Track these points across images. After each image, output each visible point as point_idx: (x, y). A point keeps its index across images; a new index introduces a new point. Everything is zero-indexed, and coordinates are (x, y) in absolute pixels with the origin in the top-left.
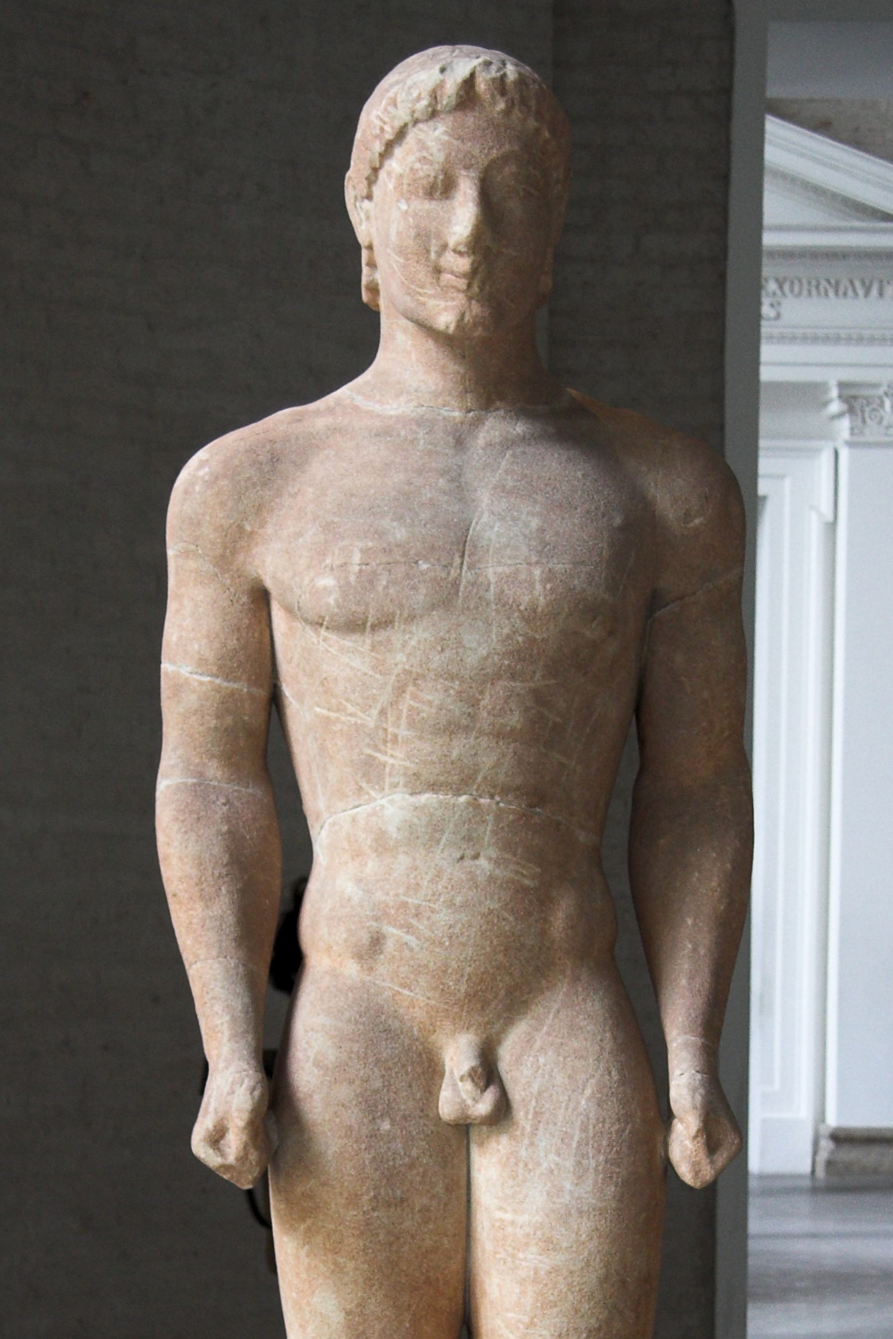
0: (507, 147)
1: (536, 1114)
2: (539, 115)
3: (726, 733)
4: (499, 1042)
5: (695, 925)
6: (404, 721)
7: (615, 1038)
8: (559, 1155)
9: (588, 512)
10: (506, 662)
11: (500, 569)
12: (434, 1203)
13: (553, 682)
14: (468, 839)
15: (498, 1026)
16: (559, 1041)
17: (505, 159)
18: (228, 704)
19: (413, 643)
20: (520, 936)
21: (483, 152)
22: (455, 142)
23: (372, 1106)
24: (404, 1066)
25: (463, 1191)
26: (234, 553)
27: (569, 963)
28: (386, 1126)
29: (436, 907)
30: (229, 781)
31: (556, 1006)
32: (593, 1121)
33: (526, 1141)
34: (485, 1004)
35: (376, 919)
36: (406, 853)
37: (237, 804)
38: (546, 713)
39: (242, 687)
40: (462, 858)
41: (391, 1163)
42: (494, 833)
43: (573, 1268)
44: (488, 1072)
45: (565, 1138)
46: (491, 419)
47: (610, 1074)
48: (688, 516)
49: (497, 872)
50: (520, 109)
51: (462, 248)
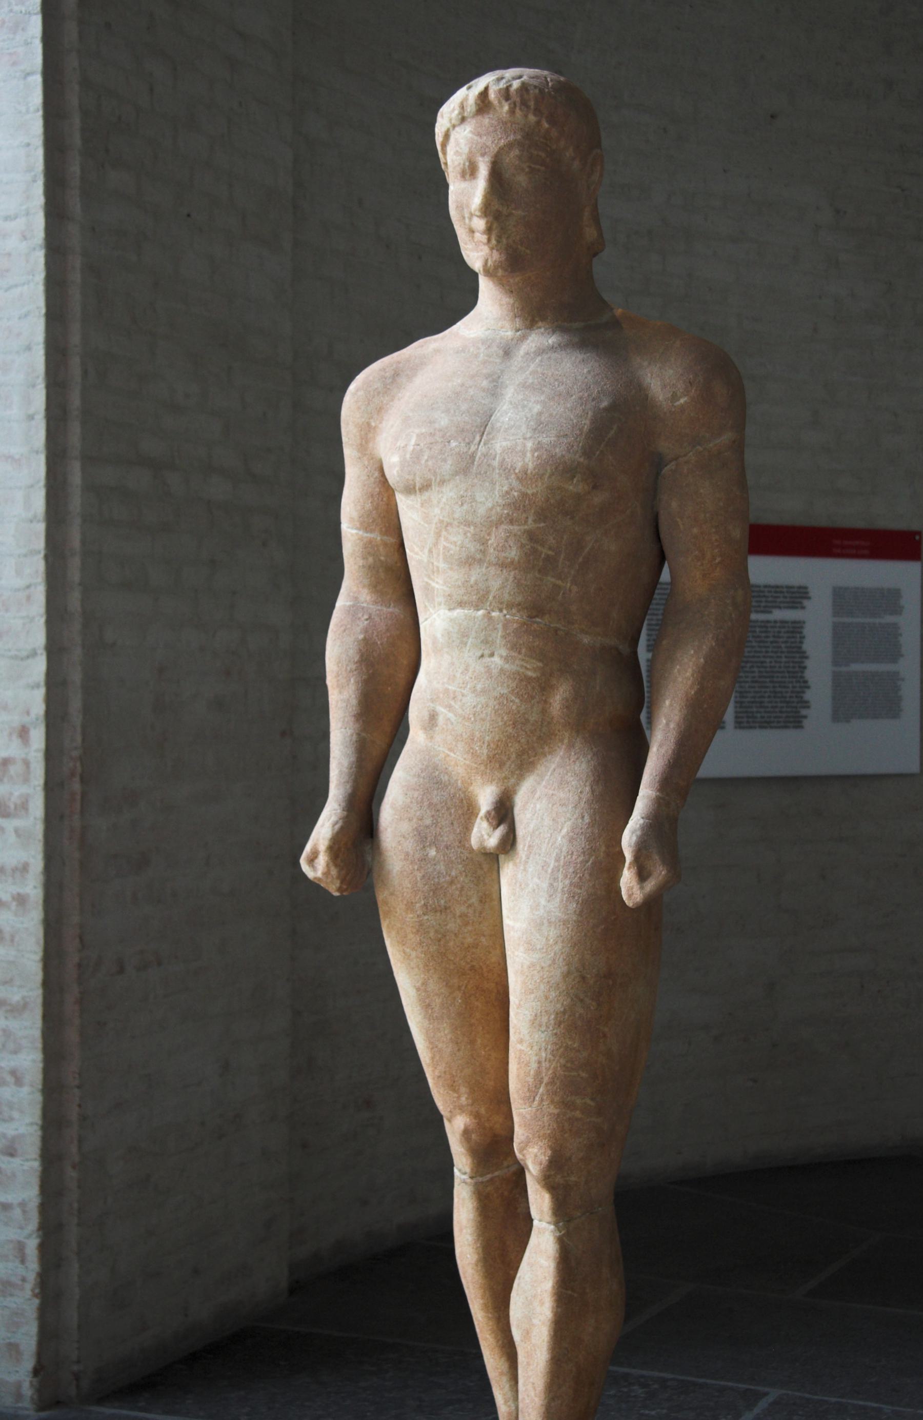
0: (511, 138)
1: (530, 846)
2: (537, 111)
3: (718, 560)
4: (515, 792)
5: (671, 705)
6: (441, 556)
7: (593, 791)
8: (539, 878)
9: (581, 398)
10: (506, 512)
11: (504, 444)
12: (471, 911)
13: (542, 525)
14: (485, 642)
15: (513, 781)
16: (551, 792)
17: (510, 146)
18: (369, 548)
19: (444, 500)
20: (524, 714)
21: (493, 143)
22: (476, 138)
23: (423, 838)
24: (448, 809)
25: (496, 903)
26: (367, 442)
27: (567, 735)
28: (433, 852)
29: (465, 692)
30: (376, 603)
31: (553, 766)
32: (564, 853)
33: (522, 868)
34: (502, 765)
35: (432, 701)
36: (447, 653)
37: (377, 619)
38: (540, 548)
39: (377, 537)
40: (482, 656)
41: (436, 880)
42: (504, 637)
43: (543, 965)
44: (503, 812)
45: (545, 865)
46: (533, 335)
47: (583, 817)
48: (674, 397)
49: (507, 666)
50: (520, 109)
51: (478, 213)
